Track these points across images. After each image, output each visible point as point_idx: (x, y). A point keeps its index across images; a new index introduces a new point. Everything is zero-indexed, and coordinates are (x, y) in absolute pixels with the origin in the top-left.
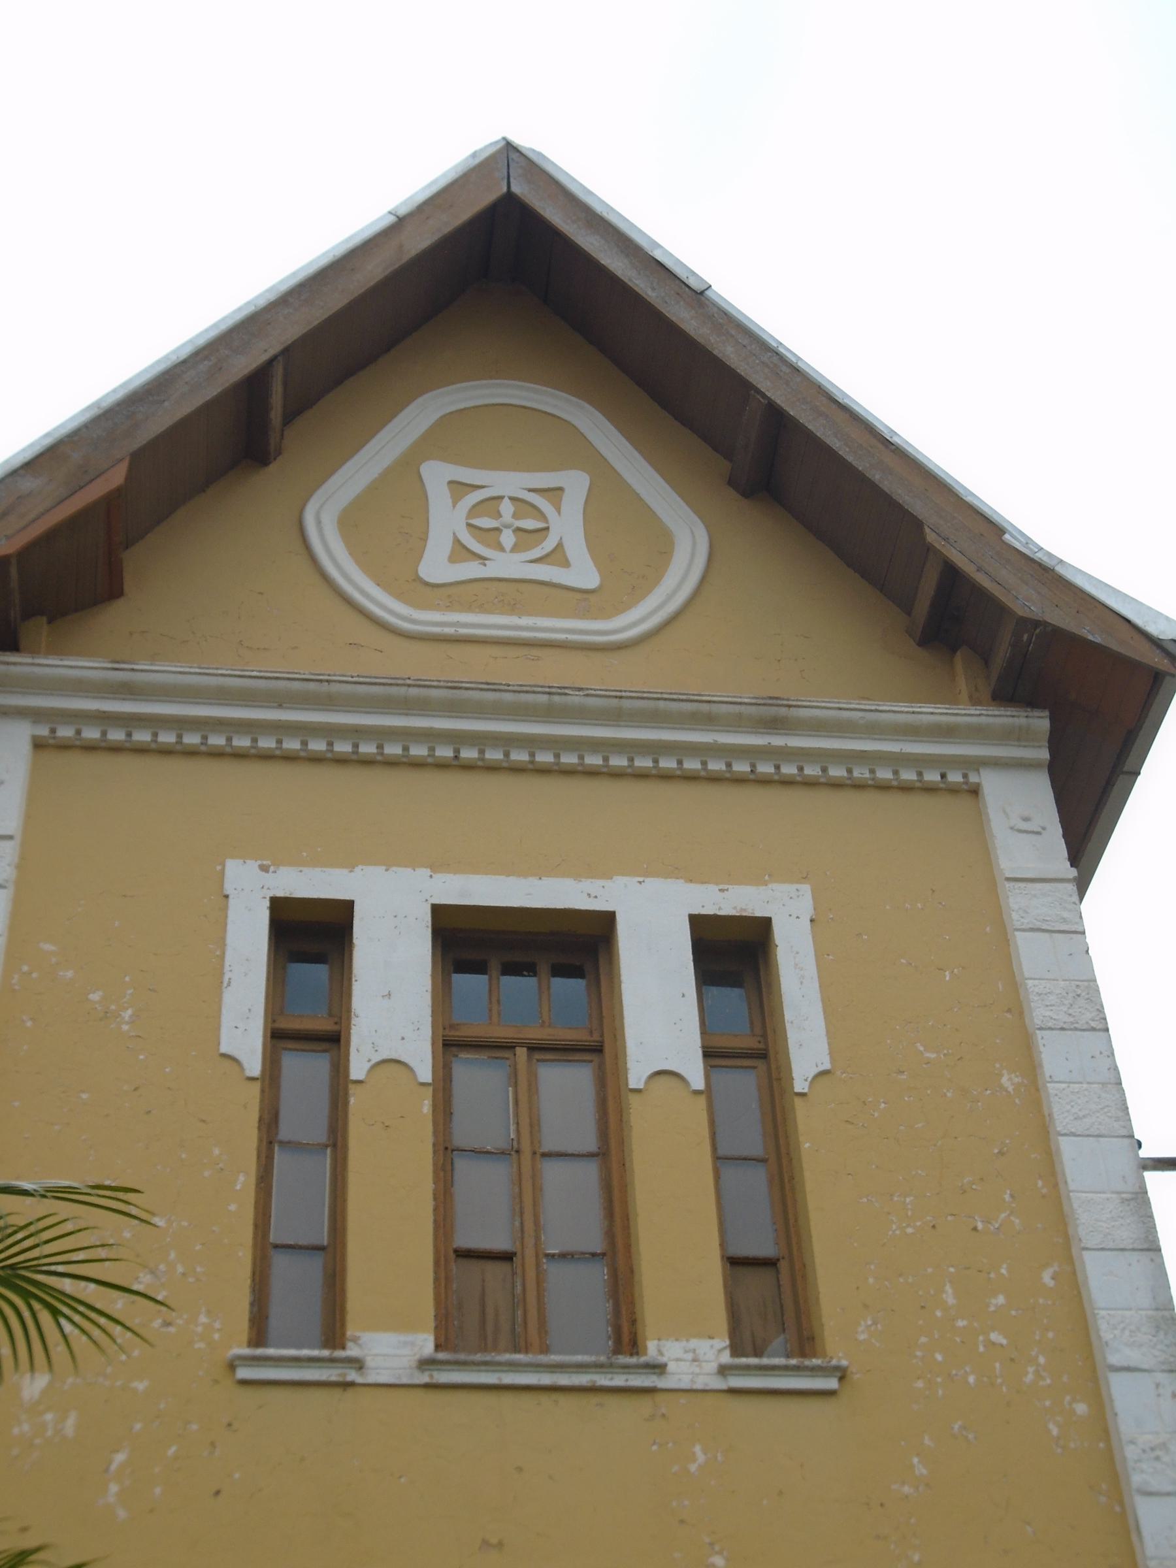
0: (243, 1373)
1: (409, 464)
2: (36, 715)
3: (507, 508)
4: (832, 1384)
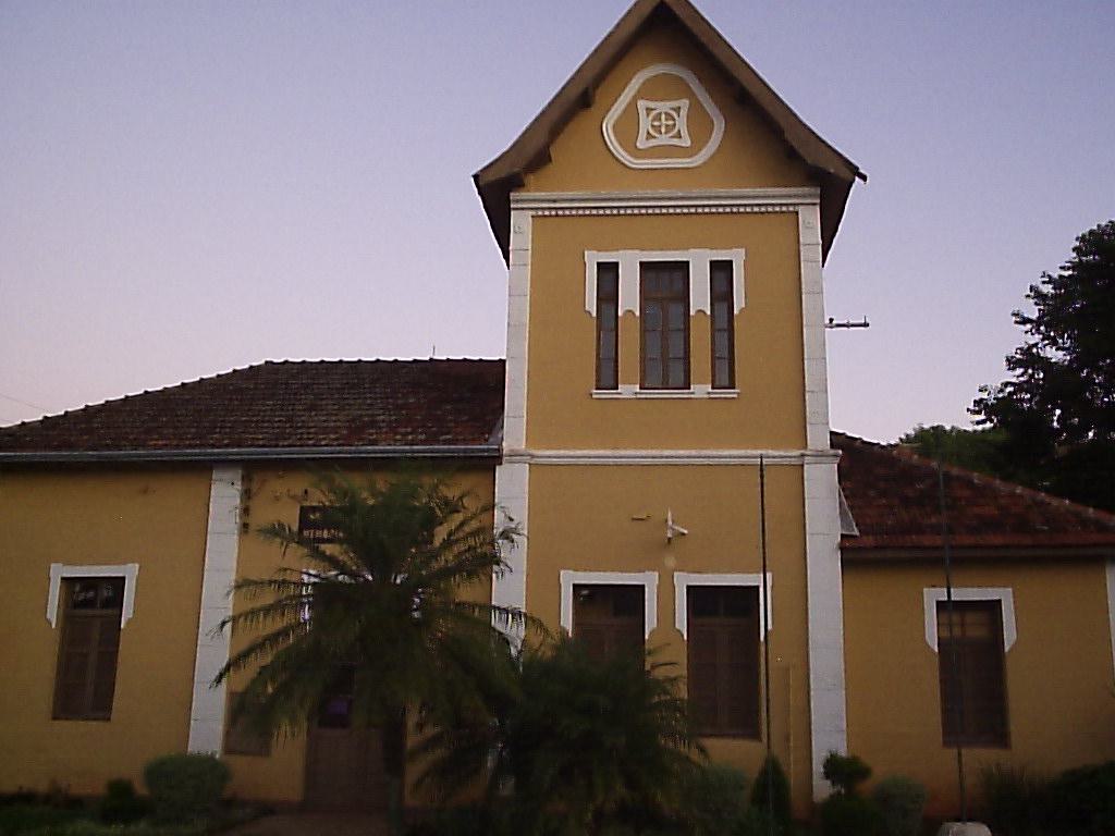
0: (594, 396)
1: (633, 105)
2: (532, 209)
3: (663, 116)
4: (735, 396)
